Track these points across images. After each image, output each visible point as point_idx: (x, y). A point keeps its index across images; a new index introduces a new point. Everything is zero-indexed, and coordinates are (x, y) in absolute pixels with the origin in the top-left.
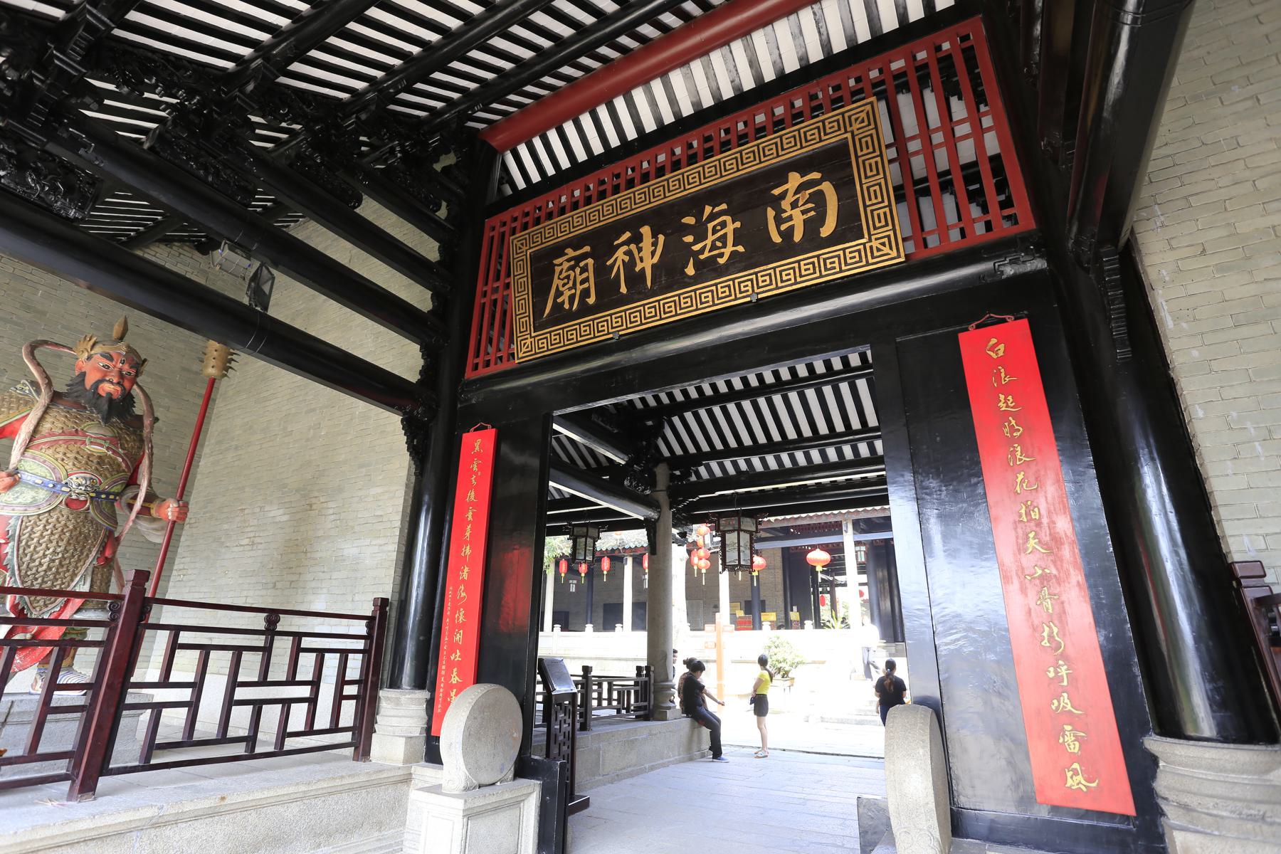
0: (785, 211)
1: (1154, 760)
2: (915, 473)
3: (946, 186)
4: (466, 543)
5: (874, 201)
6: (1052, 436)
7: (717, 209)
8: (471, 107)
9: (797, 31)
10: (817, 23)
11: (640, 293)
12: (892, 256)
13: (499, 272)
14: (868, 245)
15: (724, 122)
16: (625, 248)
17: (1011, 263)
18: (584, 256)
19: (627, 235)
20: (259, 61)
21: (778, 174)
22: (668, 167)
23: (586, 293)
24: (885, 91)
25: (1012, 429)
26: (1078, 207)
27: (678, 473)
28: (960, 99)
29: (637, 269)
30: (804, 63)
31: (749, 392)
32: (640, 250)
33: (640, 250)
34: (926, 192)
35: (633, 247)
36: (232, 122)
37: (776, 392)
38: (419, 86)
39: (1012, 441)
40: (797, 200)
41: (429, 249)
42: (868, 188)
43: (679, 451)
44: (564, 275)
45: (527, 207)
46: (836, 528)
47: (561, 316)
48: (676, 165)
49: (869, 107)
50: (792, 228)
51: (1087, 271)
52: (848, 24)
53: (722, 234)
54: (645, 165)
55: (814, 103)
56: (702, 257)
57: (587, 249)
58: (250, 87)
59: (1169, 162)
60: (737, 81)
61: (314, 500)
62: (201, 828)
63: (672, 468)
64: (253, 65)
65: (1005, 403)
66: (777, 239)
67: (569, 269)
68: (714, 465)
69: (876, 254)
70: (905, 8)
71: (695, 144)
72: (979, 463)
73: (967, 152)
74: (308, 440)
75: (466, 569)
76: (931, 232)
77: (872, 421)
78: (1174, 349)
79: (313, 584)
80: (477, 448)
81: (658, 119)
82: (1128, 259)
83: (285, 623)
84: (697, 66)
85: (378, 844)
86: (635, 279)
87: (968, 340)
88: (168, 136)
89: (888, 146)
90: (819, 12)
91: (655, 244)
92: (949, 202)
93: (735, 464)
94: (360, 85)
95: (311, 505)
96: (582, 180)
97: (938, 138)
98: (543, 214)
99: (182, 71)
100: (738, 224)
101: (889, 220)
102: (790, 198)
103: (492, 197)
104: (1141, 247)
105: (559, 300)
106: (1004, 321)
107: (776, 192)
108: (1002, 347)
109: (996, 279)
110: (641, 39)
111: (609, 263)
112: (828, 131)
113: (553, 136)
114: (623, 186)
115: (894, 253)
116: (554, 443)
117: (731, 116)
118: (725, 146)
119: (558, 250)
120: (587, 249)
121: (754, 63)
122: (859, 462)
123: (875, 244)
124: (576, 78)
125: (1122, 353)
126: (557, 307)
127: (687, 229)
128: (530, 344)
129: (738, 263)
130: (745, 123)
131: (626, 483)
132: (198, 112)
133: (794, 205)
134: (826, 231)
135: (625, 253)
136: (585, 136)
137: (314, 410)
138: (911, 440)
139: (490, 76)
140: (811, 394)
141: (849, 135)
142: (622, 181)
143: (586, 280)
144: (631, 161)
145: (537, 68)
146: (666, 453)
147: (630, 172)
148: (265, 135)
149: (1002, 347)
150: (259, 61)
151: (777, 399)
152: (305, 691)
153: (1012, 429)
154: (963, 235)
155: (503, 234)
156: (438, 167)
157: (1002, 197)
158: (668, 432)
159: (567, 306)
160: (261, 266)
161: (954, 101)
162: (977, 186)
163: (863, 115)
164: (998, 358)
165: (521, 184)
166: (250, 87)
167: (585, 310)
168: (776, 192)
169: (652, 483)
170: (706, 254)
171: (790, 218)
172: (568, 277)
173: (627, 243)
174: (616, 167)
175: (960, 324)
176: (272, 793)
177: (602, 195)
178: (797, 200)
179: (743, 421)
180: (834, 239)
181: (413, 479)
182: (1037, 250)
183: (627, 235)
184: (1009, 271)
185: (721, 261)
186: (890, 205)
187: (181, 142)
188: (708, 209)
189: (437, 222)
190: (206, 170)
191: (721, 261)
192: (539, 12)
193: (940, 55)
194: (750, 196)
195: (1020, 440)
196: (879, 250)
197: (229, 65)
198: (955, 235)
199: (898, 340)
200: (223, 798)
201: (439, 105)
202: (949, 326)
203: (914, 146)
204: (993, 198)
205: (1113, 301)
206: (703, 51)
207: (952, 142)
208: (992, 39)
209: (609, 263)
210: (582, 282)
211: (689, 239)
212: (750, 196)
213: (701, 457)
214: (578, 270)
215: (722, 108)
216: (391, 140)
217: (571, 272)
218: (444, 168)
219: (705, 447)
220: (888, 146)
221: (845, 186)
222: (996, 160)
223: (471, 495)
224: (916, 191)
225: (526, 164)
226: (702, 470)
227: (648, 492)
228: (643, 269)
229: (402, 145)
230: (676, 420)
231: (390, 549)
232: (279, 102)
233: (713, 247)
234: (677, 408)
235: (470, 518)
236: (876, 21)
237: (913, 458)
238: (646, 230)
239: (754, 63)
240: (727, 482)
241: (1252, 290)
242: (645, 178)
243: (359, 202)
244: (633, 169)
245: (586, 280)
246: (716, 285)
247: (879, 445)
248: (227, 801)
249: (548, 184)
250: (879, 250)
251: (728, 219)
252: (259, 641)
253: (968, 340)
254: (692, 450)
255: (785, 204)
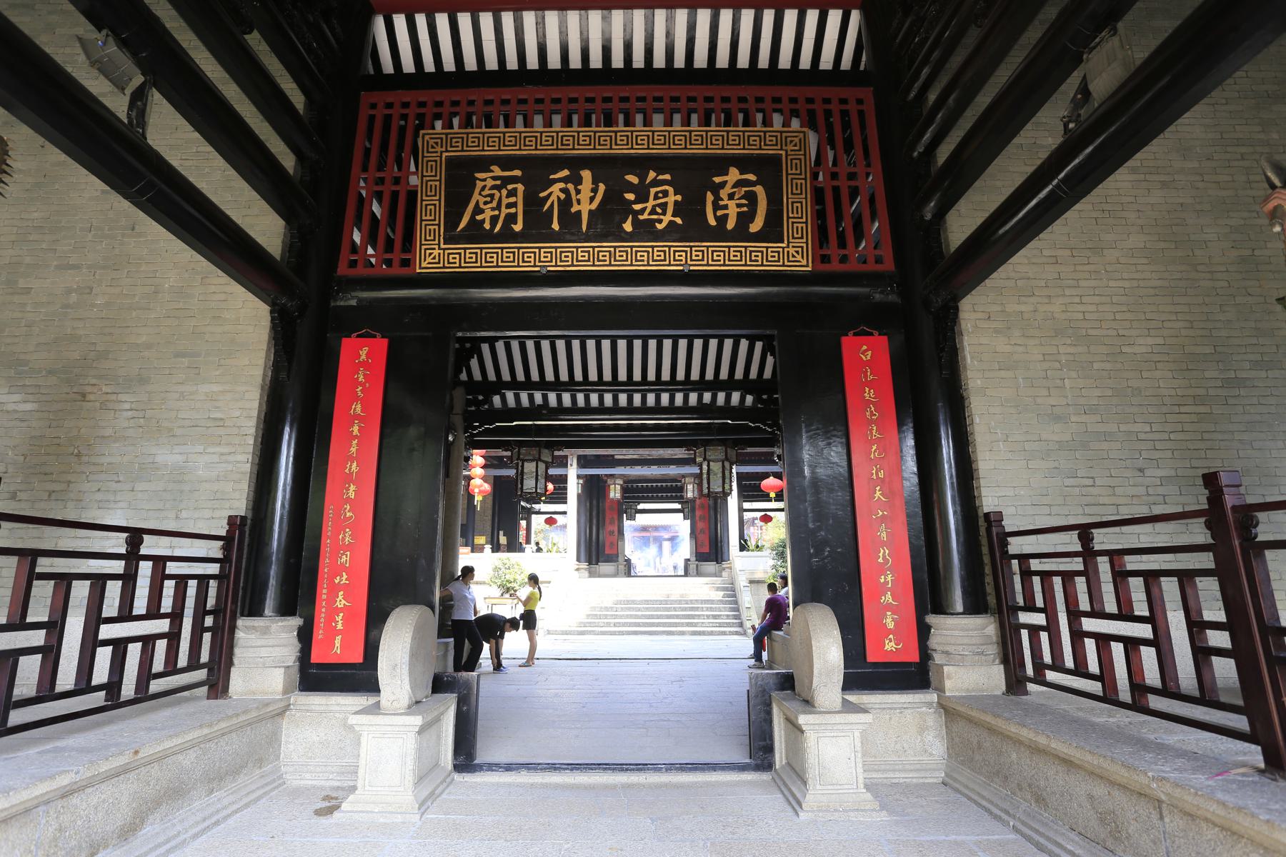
1: (929, 628)
4: (352, 459)
7: (661, 177)
11: (573, 234)
16: (562, 185)
17: (881, 292)
19: (565, 173)
21: (721, 164)
23: (511, 218)
25: (872, 414)
29: (573, 210)
32: (578, 192)
33: (578, 192)
39: (871, 422)
40: (734, 194)
44: (486, 192)
46: (563, 463)
47: (476, 234)
50: (726, 216)
53: (662, 202)
56: (641, 217)
62: (106, 792)
65: (869, 394)
66: (712, 222)
67: (493, 187)
68: (510, 396)
74: (66, 306)
75: (352, 488)
79: (99, 496)
80: (363, 357)
83: (150, 546)
85: (263, 781)
91: (595, 190)
95: (84, 395)
105: (479, 218)
106: (871, 334)
107: (717, 180)
111: (542, 195)
119: (484, 164)
123: (792, 251)
126: (475, 224)
127: (630, 187)
129: (672, 233)
133: (731, 197)
134: (755, 227)
135: (562, 190)
152: (106, 632)
153: (872, 414)
159: (487, 226)
163: (797, 140)
164: (867, 360)
167: (507, 236)
168: (717, 180)
170: (645, 216)
171: (726, 207)
172: (492, 196)
176: (180, 741)
178: (734, 194)
183: (565, 173)
184: (878, 297)
185: (660, 226)
188: (652, 175)
191: (660, 226)
194: (695, 176)
200: (136, 752)
211: (630, 197)
212: (695, 176)
214: (504, 192)
231: (243, 460)
233: (653, 212)
238: (586, 175)
240: (519, 412)
241: (1008, 349)
245: (514, 205)
248: (141, 755)
251: (671, 190)
252: (118, 567)
253: (847, 342)
255: (724, 193)
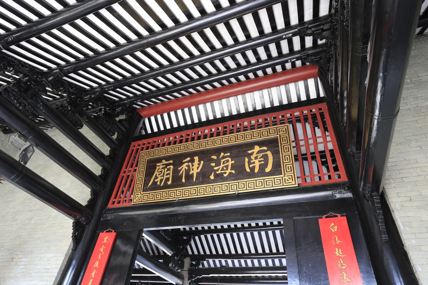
0: (252, 160)
2: (300, 280)
3: (314, 158)
5: (287, 161)
6: (359, 270)
7: (226, 155)
8: (136, 100)
9: (261, 96)
10: (269, 95)
11: (190, 183)
12: (293, 184)
13: (133, 164)
14: (284, 178)
15: (232, 123)
16: (187, 164)
17: (339, 193)
18: (170, 164)
19: (189, 159)
20: (58, 70)
21: (251, 145)
22: (208, 136)
23: (168, 179)
24: (292, 121)
26: (363, 176)
27: (194, 263)
28: (319, 128)
29: (190, 173)
30: (263, 107)
31: (230, 230)
32: (193, 166)
34: (306, 159)
35: (190, 164)
36: (39, 89)
37: (241, 231)
38: (118, 89)
39: (342, 270)
40: (257, 156)
41: (106, 150)
42: (285, 156)
43: (196, 253)
44: (160, 170)
45: (150, 140)
47: (155, 187)
48: (212, 135)
49: (286, 127)
50: (254, 167)
51: (368, 201)
52: (280, 96)
54: (200, 133)
55: (266, 122)
56: (217, 172)
57: (171, 161)
58: (51, 78)
59: (394, 164)
60: (238, 108)
61: (15, 256)
63: (192, 260)
64: (55, 71)
65: (338, 252)
66: (248, 170)
69: (287, 182)
70: (300, 95)
71: (220, 128)
72: (327, 279)
73: (321, 147)
76: (308, 176)
77: (281, 250)
78: (405, 238)
80: (105, 241)
81: (207, 117)
82: (383, 197)
84: (224, 101)
86: (189, 177)
87: (323, 222)
88: (9, 89)
89: (292, 142)
90: (270, 91)
91: (199, 164)
92: (314, 164)
93: (220, 262)
94: (95, 85)
96: (174, 134)
97: (311, 141)
98: (156, 144)
99: (24, 68)
100: (233, 162)
101: (292, 169)
102: (255, 155)
103: (137, 134)
104: (387, 194)
105: (156, 180)
106: (337, 216)
107: (250, 152)
108: (336, 227)
109: (333, 198)
110: (205, 89)
111: (179, 169)
112: (271, 133)
113: (165, 115)
114: (190, 139)
115: (294, 183)
116: (142, 243)
117: (235, 121)
118: (231, 132)
119: (159, 160)
120: (171, 161)
121: (245, 104)
122: (274, 268)
123: (287, 178)
124: (178, 97)
125: (385, 237)
126: (155, 183)
127: (213, 161)
128: (139, 197)
129: (231, 177)
130: (240, 125)
131: (170, 265)
132: (25, 83)
133: (256, 158)
134: (268, 169)
135: (187, 166)
136: (178, 118)
137: (32, 211)
138: (299, 264)
139: (146, 91)
140: (256, 234)
141: (278, 136)
142: (190, 138)
143: (169, 174)
144: (195, 131)
145: (165, 92)
146: (190, 253)
147: (193, 134)
148: (49, 95)
149: (336, 227)
150: (58, 70)
151: (242, 234)
154: (320, 179)
155: (138, 149)
156: (117, 119)
157: (334, 165)
158: (192, 243)
159: (158, 183)
160: (30, 146)
161: (316, 128)
162: (325, 160)
163: (284, 129)
164: (334, 229)
165: (149, 131)
166: (51, 78)
167: (166, 186)
168: (250, 152)
169: (182, 266)
171: (254, 163)
172: (161, 172)
173: (188, 162)
174: (189, 132)
175: (319, 215)
177: (181, 142)
178: (257, 156)
179: (226, 242)
180: (271, 174)
181: (70, 251)
182: (349, 189)
183: (189, 159)
184: (338, 196)
185: (225, 175)
186: (293, 164)
187: (14, 92)
188: (222, 154)
189: (112, 140)
190: (20, 104)
191: (225, 175)
192: (169, 74)
193: (312, 113)
194: (240, 151)
195: (345, 270)
196: (288, 180)
197: (45, 69)
198: (317, 179)
199: (294, 218)
201: (124, 97)
202: (315, 215)
203: (302, 143)
204: (331, 166)
205: (379, 214)
206: (227, 96)
207: (316, 144)
208: (330, 110)
209: (179, 169)
210: (167, 175)
212: (240, 151)
213: (205, 257)
214: (166, 169)
215: (232, 118)
216: (101, 106)
217: (163, 170)
218: (120, 120)
219: (208, 252)
220: (292, 142)
221: (276, 153)
222: (331, 151)
223: (97, 264)
224: (302, 158)
225: (153, 124)
226: (205, 263)
227: (179, 271)
228: (193, 173)
229: (105, 109)
230: (197, 238)
232: (59, 83)
233: (223, 169)
234: (198, 233)
235: (93, 276)
236: (289, 97)
237: (300, 273)
238: (196, 158)
239: (245, 104)
240: (215, 270)
242: (199, 138)
243: (82, 126)
244: (195, 134)
245: (169, 174)
246: (222, 185)
247: (284, 261)
249: (160, 133)
250: (288, 180)
251: (230, 159)
253: (323, 222)
254: (202, 253)
255: (253, 157)
